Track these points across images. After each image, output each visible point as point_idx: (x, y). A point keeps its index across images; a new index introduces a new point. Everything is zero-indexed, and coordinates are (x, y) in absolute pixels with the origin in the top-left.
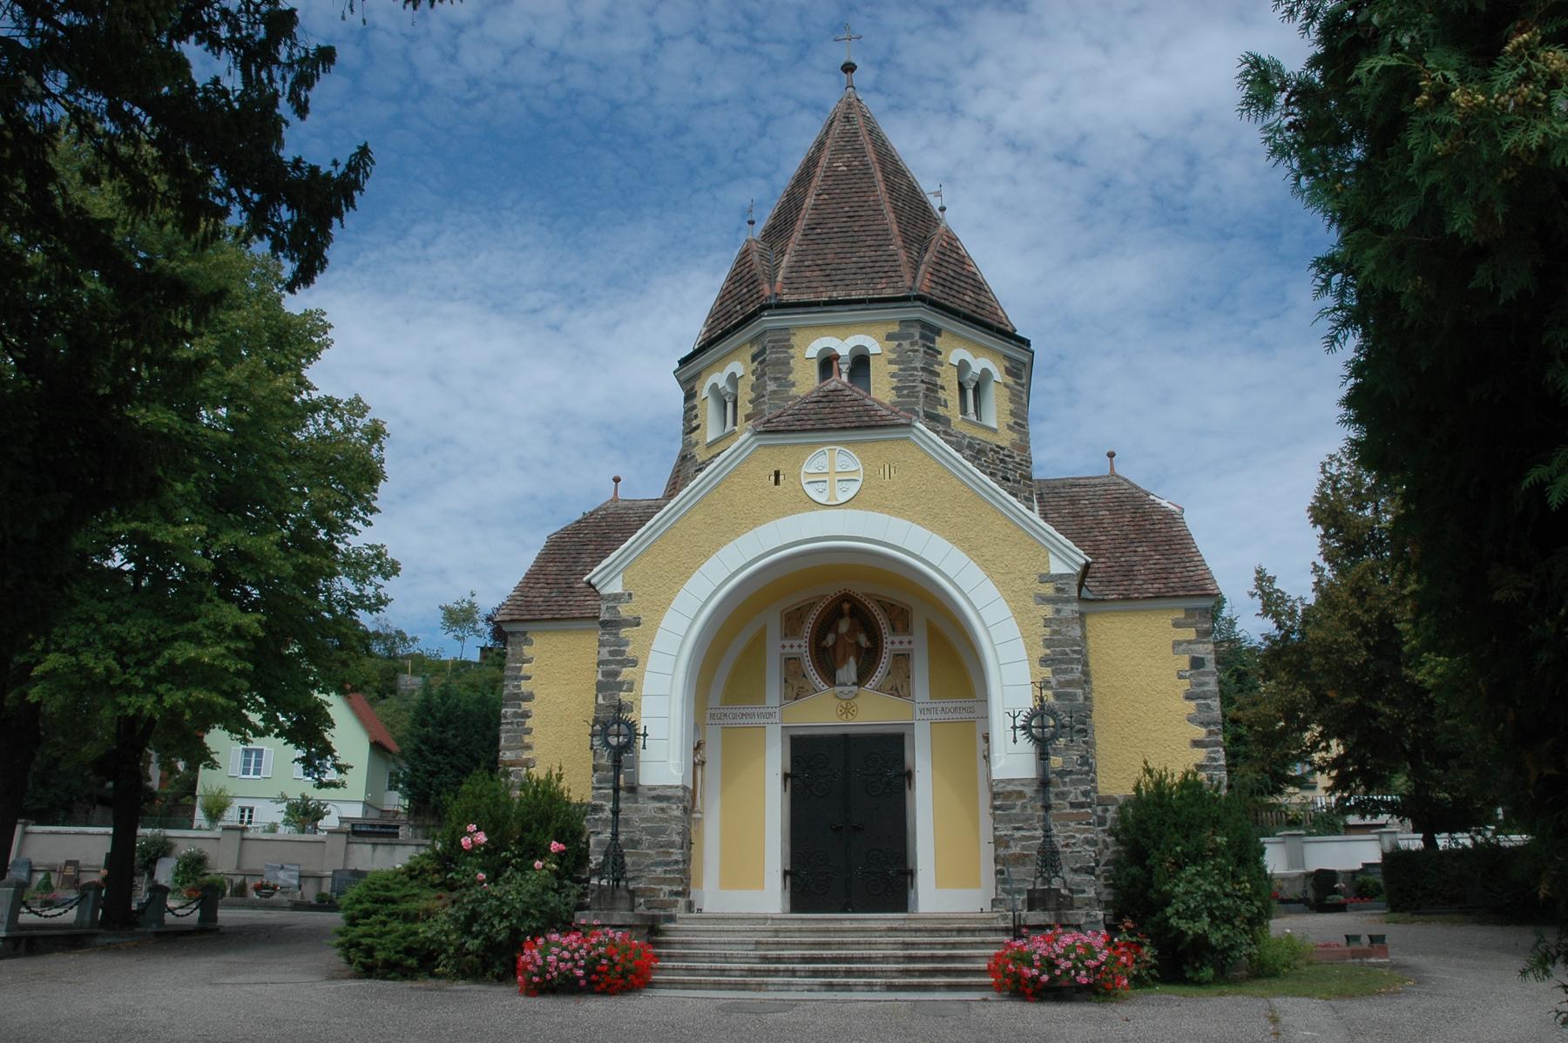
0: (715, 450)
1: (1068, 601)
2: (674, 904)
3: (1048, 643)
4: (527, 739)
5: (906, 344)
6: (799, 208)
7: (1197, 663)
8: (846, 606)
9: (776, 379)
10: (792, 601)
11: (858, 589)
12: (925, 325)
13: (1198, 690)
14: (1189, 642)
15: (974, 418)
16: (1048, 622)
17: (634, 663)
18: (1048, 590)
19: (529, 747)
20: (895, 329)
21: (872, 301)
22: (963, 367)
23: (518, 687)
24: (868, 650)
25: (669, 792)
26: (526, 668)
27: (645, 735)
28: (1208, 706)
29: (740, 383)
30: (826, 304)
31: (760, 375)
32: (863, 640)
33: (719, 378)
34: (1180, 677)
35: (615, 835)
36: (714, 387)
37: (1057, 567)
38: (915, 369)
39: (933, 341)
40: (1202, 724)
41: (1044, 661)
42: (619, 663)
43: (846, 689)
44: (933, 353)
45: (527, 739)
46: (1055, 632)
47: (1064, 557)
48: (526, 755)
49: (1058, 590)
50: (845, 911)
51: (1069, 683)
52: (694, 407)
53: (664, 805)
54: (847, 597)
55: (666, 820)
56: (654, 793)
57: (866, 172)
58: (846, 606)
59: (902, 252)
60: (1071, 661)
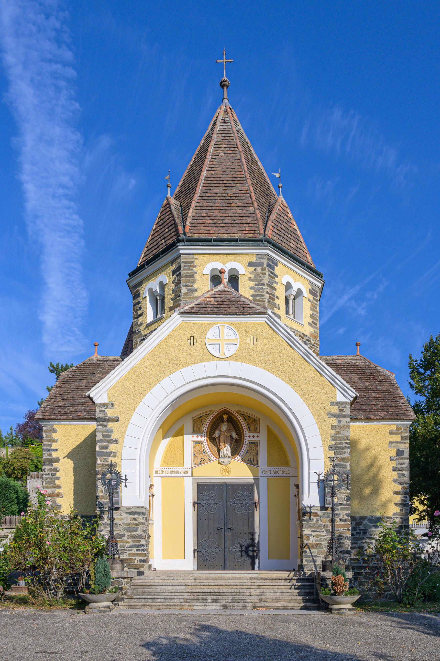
0: (152, 328)
1: (345, 416)
2: (143, 567)
3: (334, 438)
4: (57, 483)
5: (259, 270)
6: (197, 180)
7: (400, 453)
8: (225, 417)
9: (186, 286)
10: (196, 414)
11: (232, 409)
12: (270, 259)
13: (399, 466)
14: (397, 442)
15: (292, 317)
16: (334, 427)
17: (116, 442)
18: (335, 410)
19: (59, 487)
20: (253, 259)
21: (241, 241)
22: (288, 286)
23: (51, 455)
24: (236, 440)
25: (138, 510)
26: (54, 446)
27: (126, 480)
28: (403, 475)
29: (166, 287)
30: (215, 241)
31: (178, 283)
32: (234, 435)
33: (153, 284)
34: (391, 459)
35: (111, 532)
36: (151, 290)
37: (340, 398)
38: (263, 285)
39: (273, 269)
40: (400, 483)
41: (331, 448)
42: (108, 441)
43: (226, 460)
44: (273, 276)
45: (57, 483)
46: (338, 433)
47: (345, 392)
48: (57, 491)
49: (341, 410)
50: (225, 568)
51: (343, 459)
52: (139, 302)
53: (136, 516)
54: (226, 412)
55: (137, 525)
56: (130, 511)
57: (236, 158)
58: (225, 417)
59: (257, 211)
60: (344, 448)
